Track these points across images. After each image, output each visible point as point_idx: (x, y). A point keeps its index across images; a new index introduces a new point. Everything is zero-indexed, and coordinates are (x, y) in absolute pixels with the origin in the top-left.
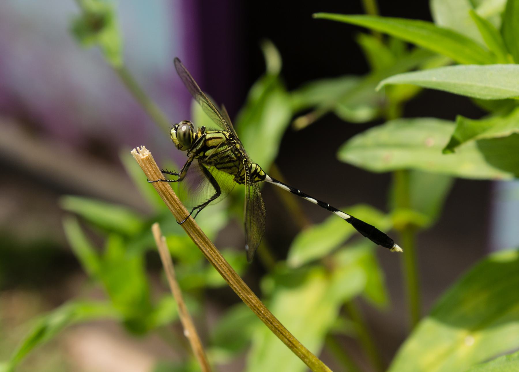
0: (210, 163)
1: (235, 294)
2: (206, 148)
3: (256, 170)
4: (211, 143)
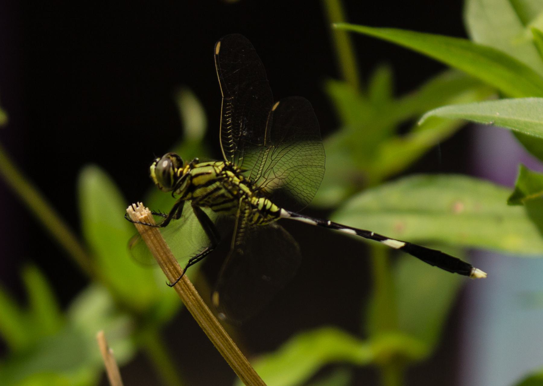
0: (203, 205)
1: (196, 321)
2: (192, 188)
3: (265, 206)
4: (196, 181)
